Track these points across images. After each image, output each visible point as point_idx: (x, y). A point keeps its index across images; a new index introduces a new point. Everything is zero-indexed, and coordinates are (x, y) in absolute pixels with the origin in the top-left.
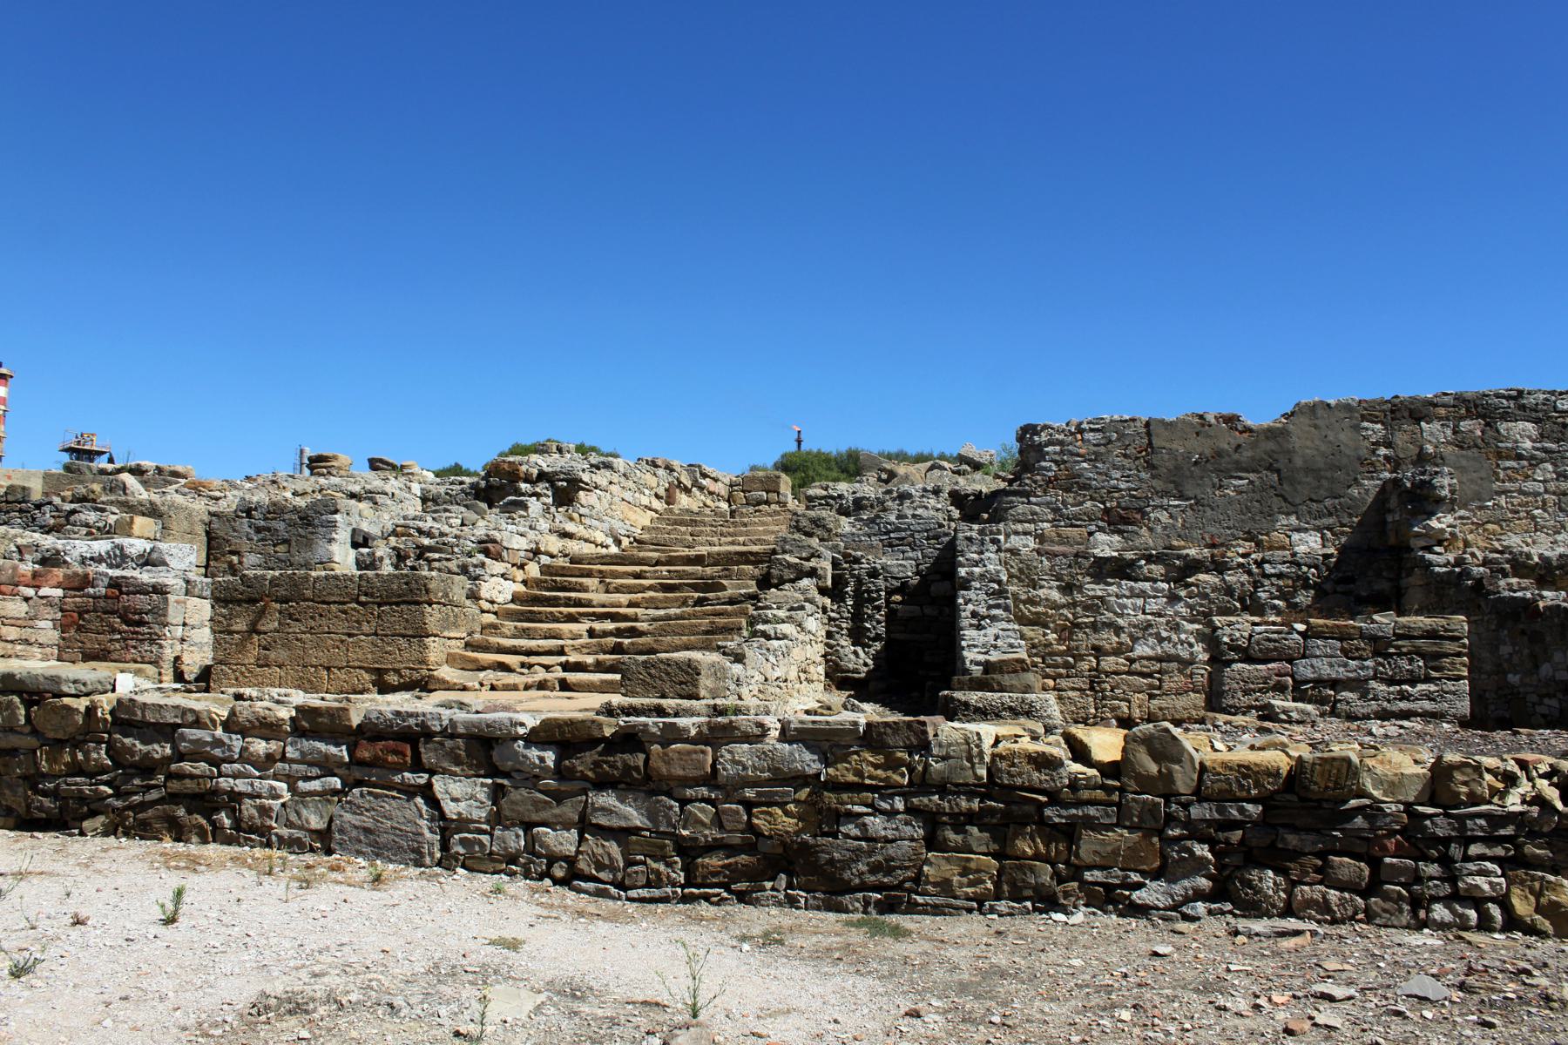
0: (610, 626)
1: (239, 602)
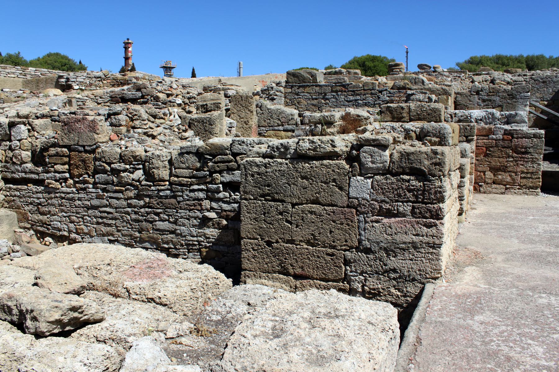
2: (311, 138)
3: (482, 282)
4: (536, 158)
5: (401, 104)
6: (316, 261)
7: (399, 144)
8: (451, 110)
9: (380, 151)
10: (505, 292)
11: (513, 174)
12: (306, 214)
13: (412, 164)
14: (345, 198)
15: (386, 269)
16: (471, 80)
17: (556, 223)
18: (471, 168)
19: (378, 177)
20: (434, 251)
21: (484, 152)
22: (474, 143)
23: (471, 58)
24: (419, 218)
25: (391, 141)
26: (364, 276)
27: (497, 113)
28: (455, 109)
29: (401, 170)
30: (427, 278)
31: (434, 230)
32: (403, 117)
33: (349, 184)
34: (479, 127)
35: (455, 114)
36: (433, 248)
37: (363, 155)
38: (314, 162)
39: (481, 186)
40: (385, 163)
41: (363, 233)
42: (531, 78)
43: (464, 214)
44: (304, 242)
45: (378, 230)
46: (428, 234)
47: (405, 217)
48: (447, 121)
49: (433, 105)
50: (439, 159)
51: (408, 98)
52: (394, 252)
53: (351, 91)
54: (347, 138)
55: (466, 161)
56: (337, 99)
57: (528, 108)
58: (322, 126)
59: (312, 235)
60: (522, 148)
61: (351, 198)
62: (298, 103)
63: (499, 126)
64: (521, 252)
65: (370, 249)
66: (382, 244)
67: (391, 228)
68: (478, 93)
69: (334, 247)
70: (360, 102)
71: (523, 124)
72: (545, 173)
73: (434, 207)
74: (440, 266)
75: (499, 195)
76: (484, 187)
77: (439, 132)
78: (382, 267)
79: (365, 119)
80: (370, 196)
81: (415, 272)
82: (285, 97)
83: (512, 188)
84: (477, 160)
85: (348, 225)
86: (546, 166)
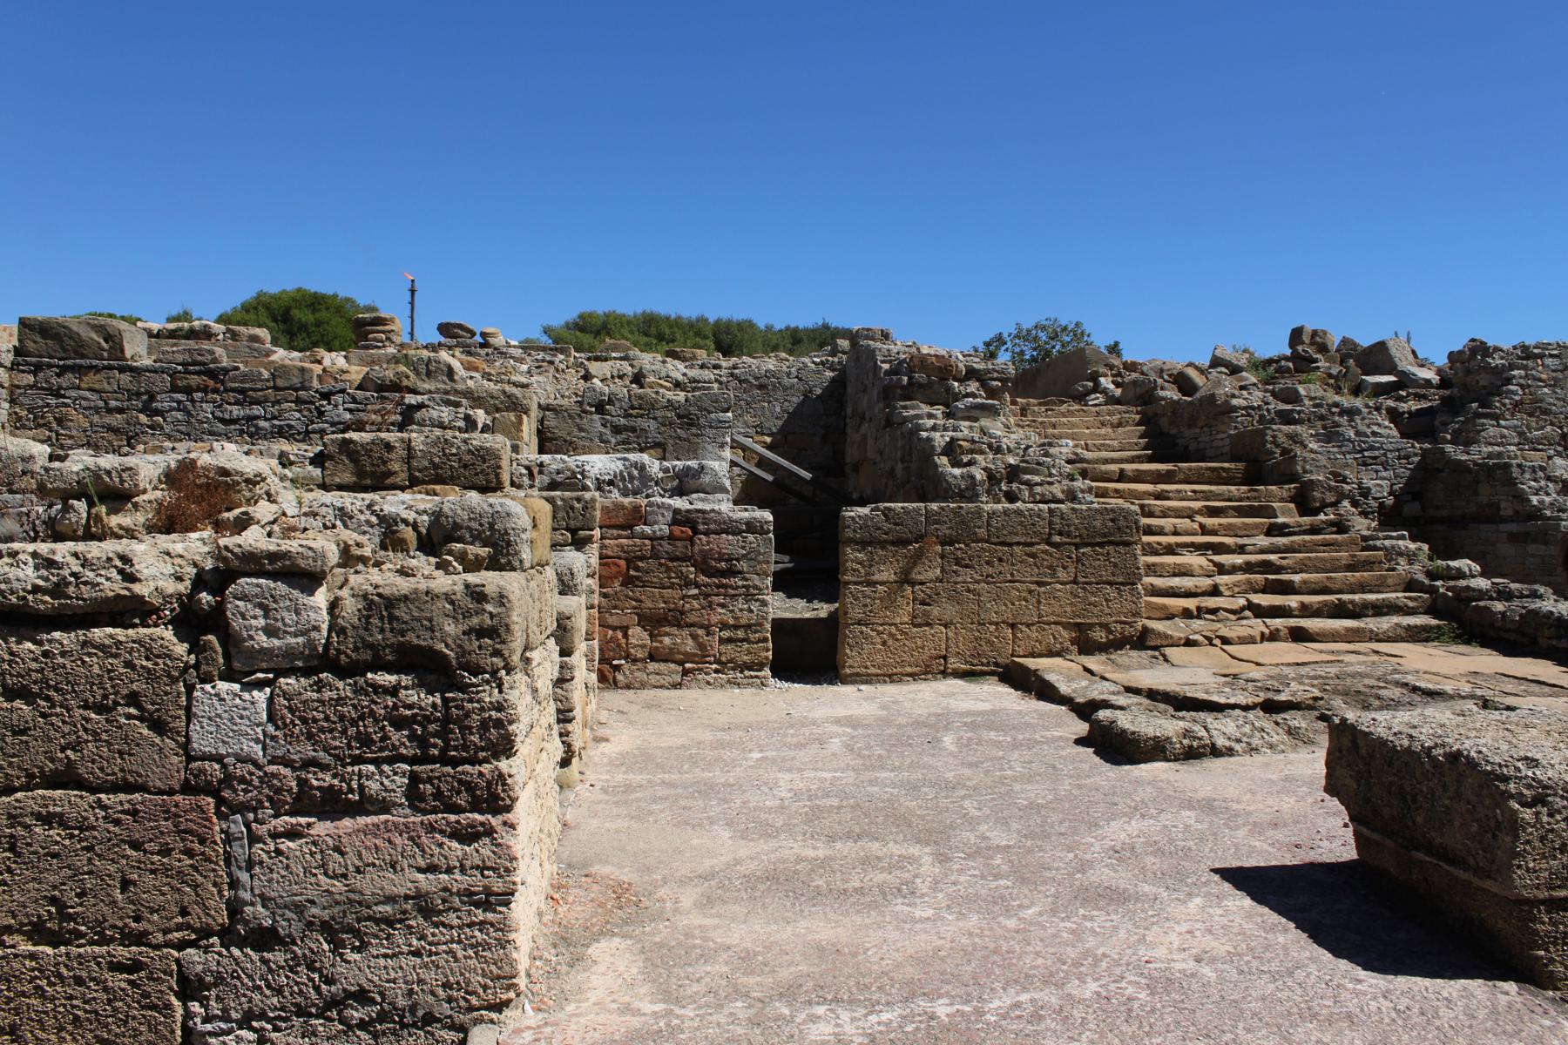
0: (1239, 560)
1: (882, 544)
2: (43, 548)
3: (643, 990)
4: (756, 587)
5: (383, 435)
6: (71, 998)
7: (360, 567)
8: (530, 454)
9: (296, 593)
10: (714, 1018)
11: (700, 632)
12: (27, 827)
13: (403, 633)
14: (175, 759)
15: (333, 996)
16: (582, 372)
17: (820, 765)
18: (588, 621)
19: (289, 682)
20: (490, 916)
21: (622, 574)
22: (594, 549)
23: (581, 317)
24: (434, 811)
25: (333, 555)
26: (255, 1030)
27: (654, 467)
28: (541, 451)
29: (367, 656)
30: (471, 1009)
31: (484, 848)
32: (391, 474)
33: (188, 709)
34: (607, 502)
35: (541, 465)
36: (487, 906)
37: (235, 606)
38: (57, 635)
39: (617, 668)
40: (314, 634)
41: (244, 877)
42: (732, 375)
43: (575, 761)
44: (19, 932)
45: (299, 864)
46: (468, 863)
47: (386, 811)
48: (519, 487)
49: (478, 439)
50: (492, 616)
51: (408, 417)
52: (356, 933)
53: (233, 390)
54: (179, 548)
55: (575, 604)
56: (189, 414)
57: (727, 453)
58: (91, 505)
59: (53, 901)
60: (720, 560)
61: (195, 759)
62: (60, 421)
63: (658, 499)
64: (741, 869)
65: (273, 930)
66: (314, 911)
67: (342, 854)
68: (600, 408)
69: (140, 939)
70: (262, 423)
71: (719, 496)
72: (778, 624)
73: (481, 774)
74: (512, 963)
75: (666, 693)
76: (627, 672)
77: (491, 525)
78: (317, 989)
79: (247, 481)
80: (264, 749)
81: (433, 993)
82: (12, 401)
83: (700, 670)
84: (605, 596)
85: (189, 853)
86: (782, 607)
